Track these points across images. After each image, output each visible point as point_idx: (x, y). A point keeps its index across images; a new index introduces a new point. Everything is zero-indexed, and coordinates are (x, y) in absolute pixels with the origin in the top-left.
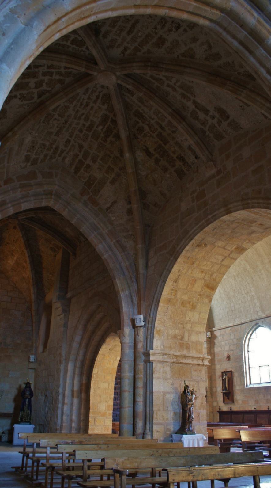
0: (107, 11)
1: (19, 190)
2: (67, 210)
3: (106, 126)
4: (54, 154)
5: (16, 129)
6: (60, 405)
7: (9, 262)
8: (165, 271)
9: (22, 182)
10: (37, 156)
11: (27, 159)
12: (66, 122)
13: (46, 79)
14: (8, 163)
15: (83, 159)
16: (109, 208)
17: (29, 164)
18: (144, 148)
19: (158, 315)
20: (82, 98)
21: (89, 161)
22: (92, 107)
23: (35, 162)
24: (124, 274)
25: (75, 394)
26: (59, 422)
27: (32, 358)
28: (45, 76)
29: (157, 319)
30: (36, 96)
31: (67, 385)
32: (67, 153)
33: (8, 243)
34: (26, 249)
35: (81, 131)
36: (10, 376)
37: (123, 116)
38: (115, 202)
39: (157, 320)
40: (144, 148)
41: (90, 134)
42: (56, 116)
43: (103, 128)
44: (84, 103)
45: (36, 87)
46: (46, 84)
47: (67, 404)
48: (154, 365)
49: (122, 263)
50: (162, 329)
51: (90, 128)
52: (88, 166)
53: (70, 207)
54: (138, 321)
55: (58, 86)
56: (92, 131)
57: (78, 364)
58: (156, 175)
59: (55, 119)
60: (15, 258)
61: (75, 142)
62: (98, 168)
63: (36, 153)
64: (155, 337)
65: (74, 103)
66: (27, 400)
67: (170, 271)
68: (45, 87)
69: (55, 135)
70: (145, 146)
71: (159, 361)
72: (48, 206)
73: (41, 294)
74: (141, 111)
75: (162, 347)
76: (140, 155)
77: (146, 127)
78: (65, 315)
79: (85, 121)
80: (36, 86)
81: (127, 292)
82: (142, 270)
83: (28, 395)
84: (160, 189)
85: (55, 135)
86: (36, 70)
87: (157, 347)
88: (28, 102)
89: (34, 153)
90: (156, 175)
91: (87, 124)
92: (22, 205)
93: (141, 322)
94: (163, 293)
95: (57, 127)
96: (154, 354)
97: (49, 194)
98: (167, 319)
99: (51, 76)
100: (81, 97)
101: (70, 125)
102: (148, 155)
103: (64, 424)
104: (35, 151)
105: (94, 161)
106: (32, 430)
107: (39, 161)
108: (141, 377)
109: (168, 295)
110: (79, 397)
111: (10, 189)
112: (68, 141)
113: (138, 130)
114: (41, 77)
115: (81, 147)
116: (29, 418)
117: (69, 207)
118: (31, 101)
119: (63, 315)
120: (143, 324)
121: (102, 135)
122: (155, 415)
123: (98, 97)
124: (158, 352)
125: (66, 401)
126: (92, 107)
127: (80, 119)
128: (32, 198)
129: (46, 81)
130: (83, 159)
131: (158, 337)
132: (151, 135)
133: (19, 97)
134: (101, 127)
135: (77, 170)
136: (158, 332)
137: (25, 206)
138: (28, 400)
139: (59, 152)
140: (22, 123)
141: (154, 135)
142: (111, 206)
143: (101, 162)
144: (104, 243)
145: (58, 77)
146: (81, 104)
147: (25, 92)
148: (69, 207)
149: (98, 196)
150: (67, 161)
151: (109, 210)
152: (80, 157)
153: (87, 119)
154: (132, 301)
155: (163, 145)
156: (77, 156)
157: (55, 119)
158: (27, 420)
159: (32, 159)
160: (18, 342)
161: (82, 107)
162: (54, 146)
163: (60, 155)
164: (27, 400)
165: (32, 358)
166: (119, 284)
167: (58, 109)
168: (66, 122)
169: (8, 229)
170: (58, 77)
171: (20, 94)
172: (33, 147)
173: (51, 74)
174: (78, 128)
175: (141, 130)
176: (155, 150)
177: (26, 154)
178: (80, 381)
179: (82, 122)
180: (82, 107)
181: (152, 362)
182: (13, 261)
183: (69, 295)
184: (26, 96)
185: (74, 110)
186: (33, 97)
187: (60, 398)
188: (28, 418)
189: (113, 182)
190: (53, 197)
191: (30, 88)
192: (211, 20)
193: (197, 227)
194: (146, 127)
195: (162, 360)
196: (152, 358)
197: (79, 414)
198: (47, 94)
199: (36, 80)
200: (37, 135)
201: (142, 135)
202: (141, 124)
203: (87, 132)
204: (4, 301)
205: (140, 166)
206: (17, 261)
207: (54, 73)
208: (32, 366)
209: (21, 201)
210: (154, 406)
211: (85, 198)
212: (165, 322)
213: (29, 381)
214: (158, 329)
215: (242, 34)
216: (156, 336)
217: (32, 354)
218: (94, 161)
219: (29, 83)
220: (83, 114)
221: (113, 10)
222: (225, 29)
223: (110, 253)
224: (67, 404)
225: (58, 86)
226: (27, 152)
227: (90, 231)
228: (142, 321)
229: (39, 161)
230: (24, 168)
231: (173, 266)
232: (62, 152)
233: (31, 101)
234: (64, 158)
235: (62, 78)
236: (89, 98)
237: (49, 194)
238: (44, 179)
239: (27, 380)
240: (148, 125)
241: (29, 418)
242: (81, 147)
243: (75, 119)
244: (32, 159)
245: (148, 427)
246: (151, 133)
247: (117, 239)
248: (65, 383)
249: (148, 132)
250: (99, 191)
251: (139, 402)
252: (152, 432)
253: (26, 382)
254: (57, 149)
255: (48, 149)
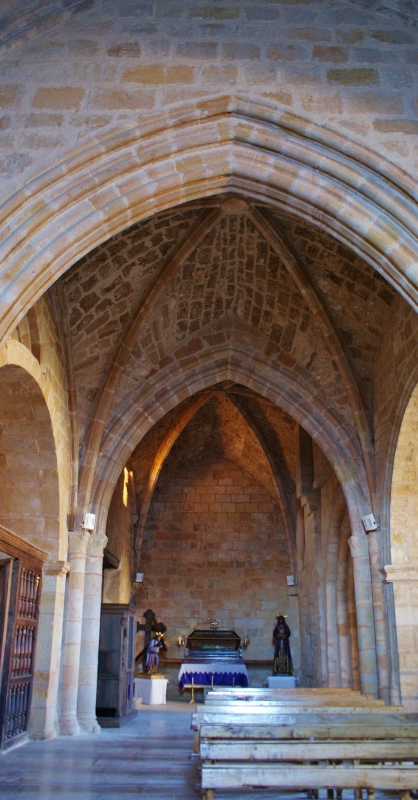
0: (37, 292)
1: (181, 370)
2: (251, 380)
3: (268, 258)
4: (218, 308)
5: (147, 301)
6: (323, 647)
7: (236, 446)
8: (390, 447)
9: (183, 359)
10: (195, 319)
11: (182, 326)
12: (215, 267)
13: (163, 230)
14: (157, 340)
15: (257, 305)
16: (309, 365)
17: (188, 331)
18: (327, 273)
19: (392, 512)
20: (222, 233)
21: (265, 307)
22: (241, 239)
23: (195, 327)
24: (345, 456)
25: (342, 631)
26: (324, 671)
27: (290, 580)
28: (159, 228)
29: (392, 518)
30: (159, 253)
31: (329, 617)
32: (236, 302)
33: (226, 421)
34: (250, 426)
35: (241, 271)
36: (262, 608)
37: (279, 242)
38: (314, 355)
39: (394, 520)
40: (327, 273)
41: (253, 271)
42: (198, 265)
43: (265, 261)
44: (228, 238)
45: (155, 245)
46: (166, 235)
47: (331, 645)
48: (395, 586)
49: (340, 440)
50: (403, 531)
51: (250, 264)
52: (267, 314)
53: (255, 375)
54: (367, 523)
55: (183, 233)
56: (254, 268)
57: (340, 585)
58: (356, 307)
59: (199, 269)
60: (243, 440)
61: (241, 286)
62: (279, 314)
63: (191, 316)
64: (392, 545)
65: (215, 242)
66: (282, 642)
67: (395, 446)
68: (166, 240)
69: (209, 287)
70: (327, 270)
71: (402, 581)
72: (226, 380)
73: (287, 487)
74: (303, 227)
75: (407, 558)
76: (324, 284)
77: (319, 245)
78: (315, 515)
79: (240, 258)
80: (154, 243)
81: (353, 482)
82: (365, 449)
83: (282, 634)
84: (367, 324)
85: (209, 287)
86: (146, 226)
87: (398, 559)
88: (152, 264)
89: (189, 317)
90: (356, 307)
91: (245, 260)
92: (189, 388)
93: (371, 525)
94: (394, 480)
95: (206, 276)
96: (393, 571)
97: (223, 364)
98: (409, 515)
99: (168, 225)
100: (219, 233)
101: (223, 268)
102: (335, 282)
103: (330, 675)
104: (189, 315)
105: (272, 306)
106: (293, 684)
107: (201, 323)
108: (379, 605)
109: (403, 480)
110: (347, 634)
111: (168, 372)
112: (231, 288)
113: (309, 251)
114: (156, 232)
115: (249, 290)
116: (288, 666)
117: (253, 376)
118: (157, 261)
119: (312, 516)
120: (375, 527)
121: (268, 270)
122: (402, 661)
123: (242, 225)
124: (398, 567)
125: (330, 641)
126: (241, 239)
127: (232, 257)
128: (201, 376)
129: (164, 233)
130: (257, 305)
131: (399, 544)
132: (330, 254)
133: (138, 263)
134: (262, 261)
135: (255, 321)
136: (397, 537)
137: (192, 390)
138: (283, 642)
139: (224, 304)
140: (152, 292)
141: (334, 252)
142: (311, 361)
143: (279, 305)
144: (310, 417)
145: (177, 223)
146: (225, 241)
147: (143, 255)
148: (253, 376)
149: (292, 351)
150: (240, 312)
151: (310, 368)
152: (253, 303)
153: (241, 255)
154: (362, 494)
155: (350, 263)
156: (248, 303)
157: (199, 269)
158: (284, 670)
159: (189, 325)
160: (269, 558)
161: (228, 242)
162: (214, 300)
163: (228, 307)
164: (282, 642)
165: (290, 580)
166: (341, 471)
167: (197, 257)
168: (215, 267)
169: (220, 403)
170: (177, 223)
171: (138, 259)
172: (184, 310)
173: (167, 223)
174: (235, 268)
175: (313, 250)
176: (342, 272)
177: (178, 321)
178: (347, 610)
179: (237, 260)
180: (228, 242)
181: (392, 583)
182: (242, 444)
183: (315, 485)
184: (146, 258)
185: (218, 250)
186: (157, 256)
187: (322, 636)
188: (286, 667)
189: (303, 328)
190: (229, 367)
191: (148, 248)
192: (223, 187)
193: (411, 378)
194: (319, 245)
195: (406, 578)
196: (389, 578)
197: (350, 659)
198: (174, 246)
199: (150, 237)
200: (182, 295)
201: (318, 256)
202: (310, 243)
203: (248, 271)
204: (240, 503)
205: (329, 299)
206: (245, 443)
207: (171, 220)
208: (292, 591)
209: (187, 383)
210: (399, 648)
211: (274, 357)
212: (406, 521)
213: (282, 615)
214: (396, 532)
215: (263, 188)
216: (394, 543)
217: (290, 574)
218: (272, 306)
219: (143, 243)
220: (233, 251)
221: (80, 252)
222: (243, 189)
223: (321, 429)
224: (331, 645)
225: (183, 233)
226: (178, 318)
227: (288, 403)
228: (373, 524)
229: (201, 323)
230: (182, 339)
231: (397, 440)
232: (229, 302)
233: (157, 261)
234: (235, 309)
235: (182, 222)
236: (231, 230)
237: (223, 364)
238: (212, 347)
239: (279, 613)
240: (320, 241)
241: (288, 666)
242: (249, 290)
243: (226, 259)
244: (189, 325)
245: (394, 678)
246: (328, 251)
247: (329, 407)
248: (325, 614)
249: (324, 251)
250: (291, 344)
251: (381, 641)
252: (399, 684)
253: (278, 615)
254: (219, 301)
255: (206, 306)
